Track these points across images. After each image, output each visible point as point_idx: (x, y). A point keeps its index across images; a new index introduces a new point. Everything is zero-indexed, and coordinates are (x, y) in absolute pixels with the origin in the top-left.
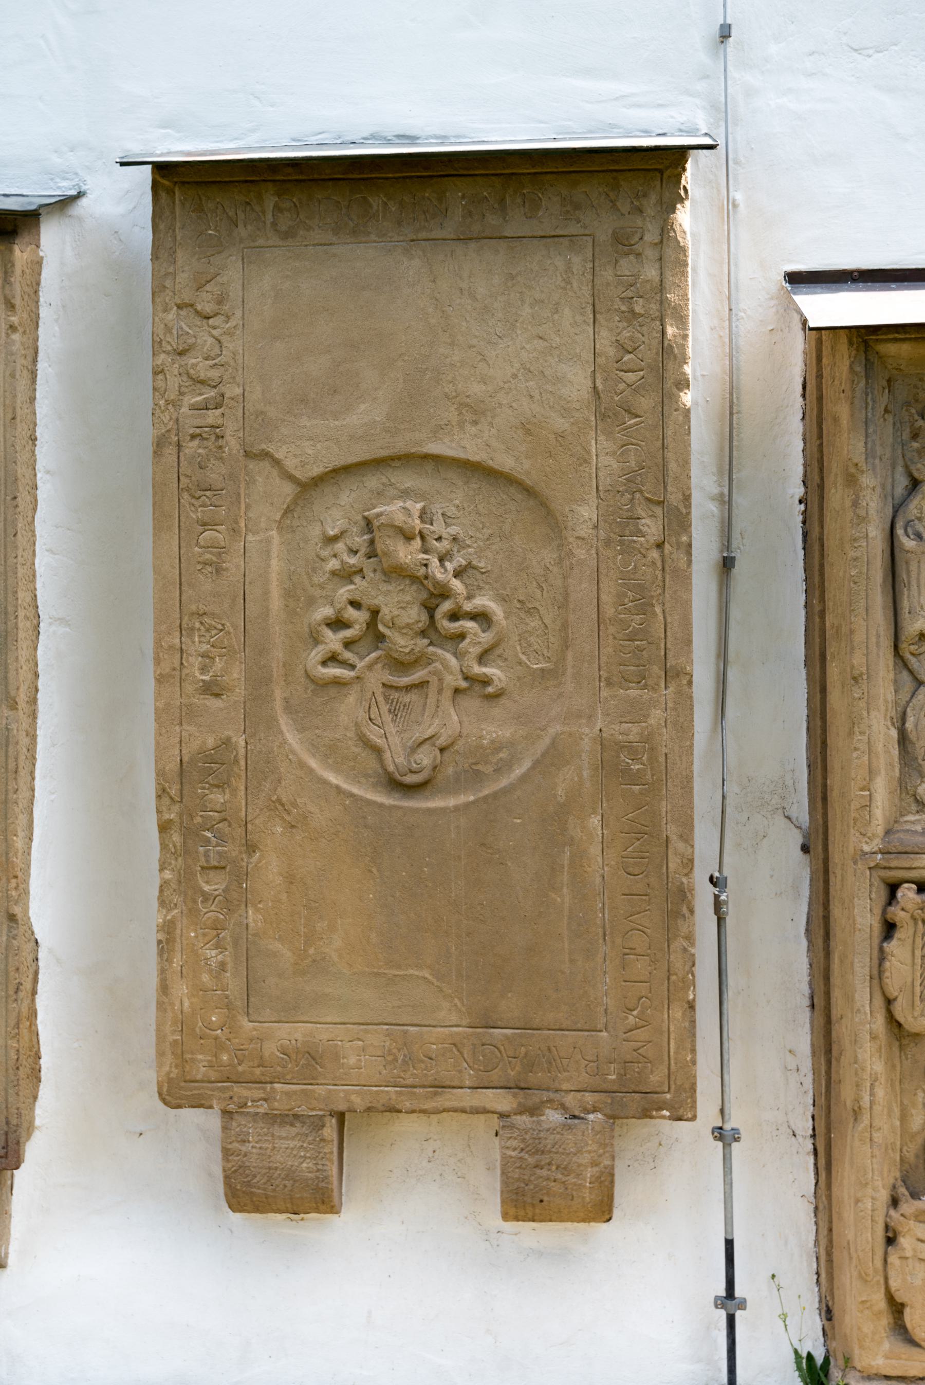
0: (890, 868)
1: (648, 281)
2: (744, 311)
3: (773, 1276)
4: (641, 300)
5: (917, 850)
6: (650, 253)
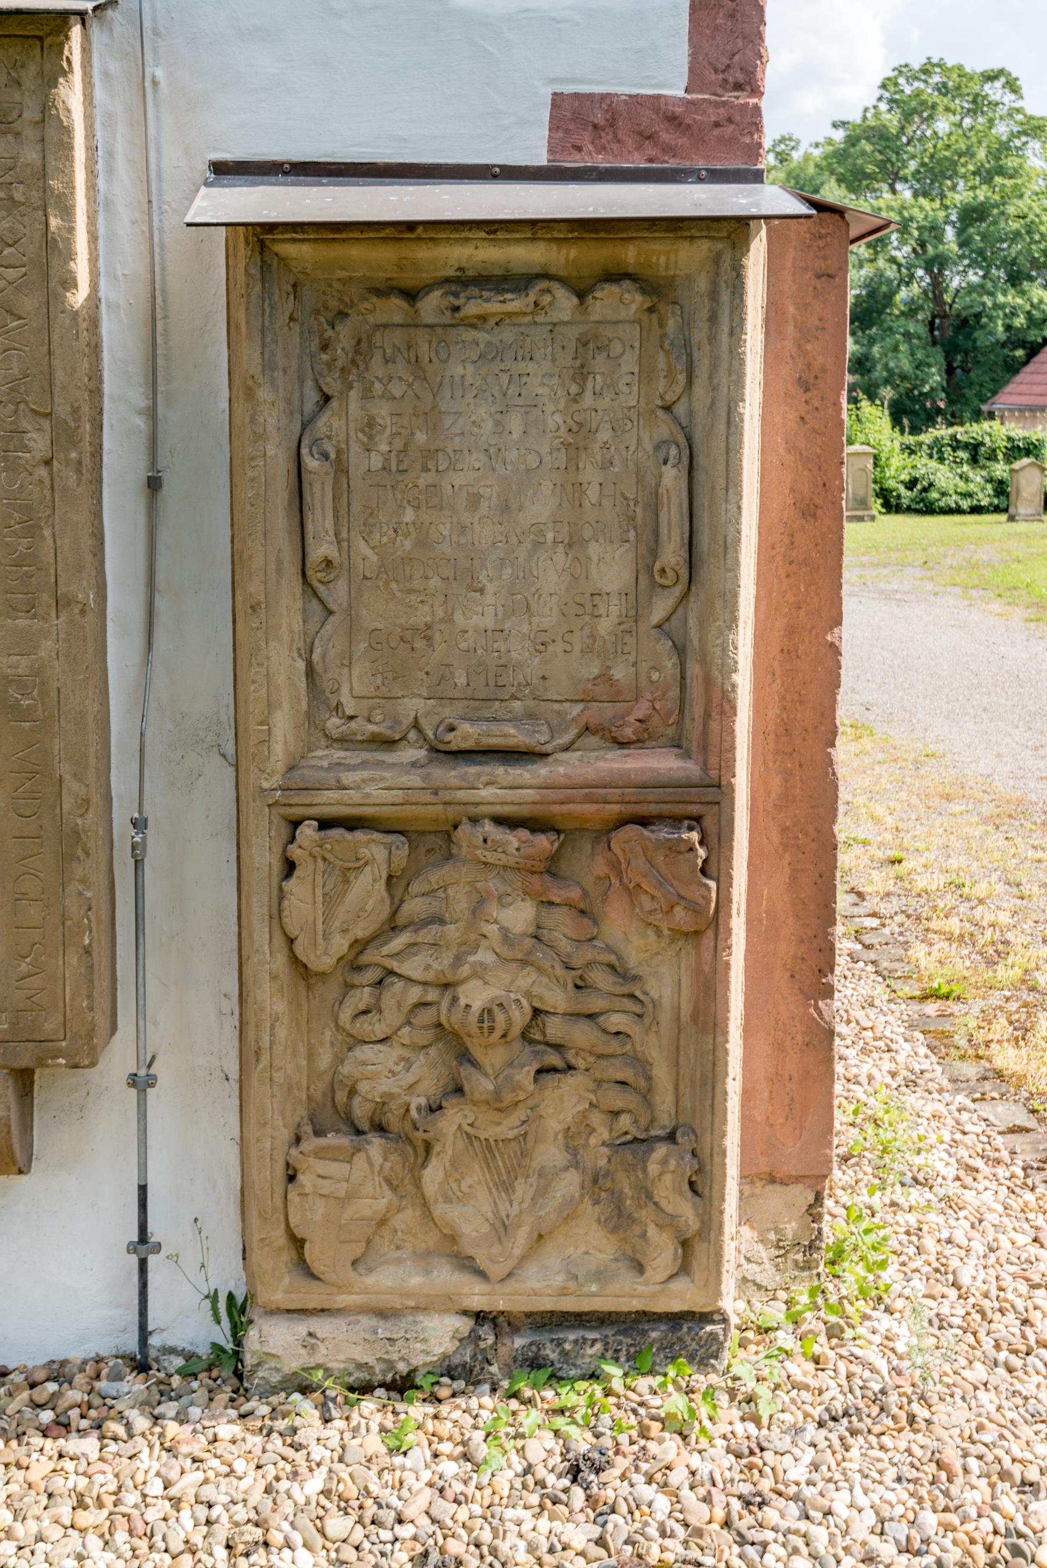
0: (290, 805)
1: (28, 165)
2: (168, 203)
3: (196, 1220)
4: (21, 186)
5: (318, 786)
6: (30, 133)
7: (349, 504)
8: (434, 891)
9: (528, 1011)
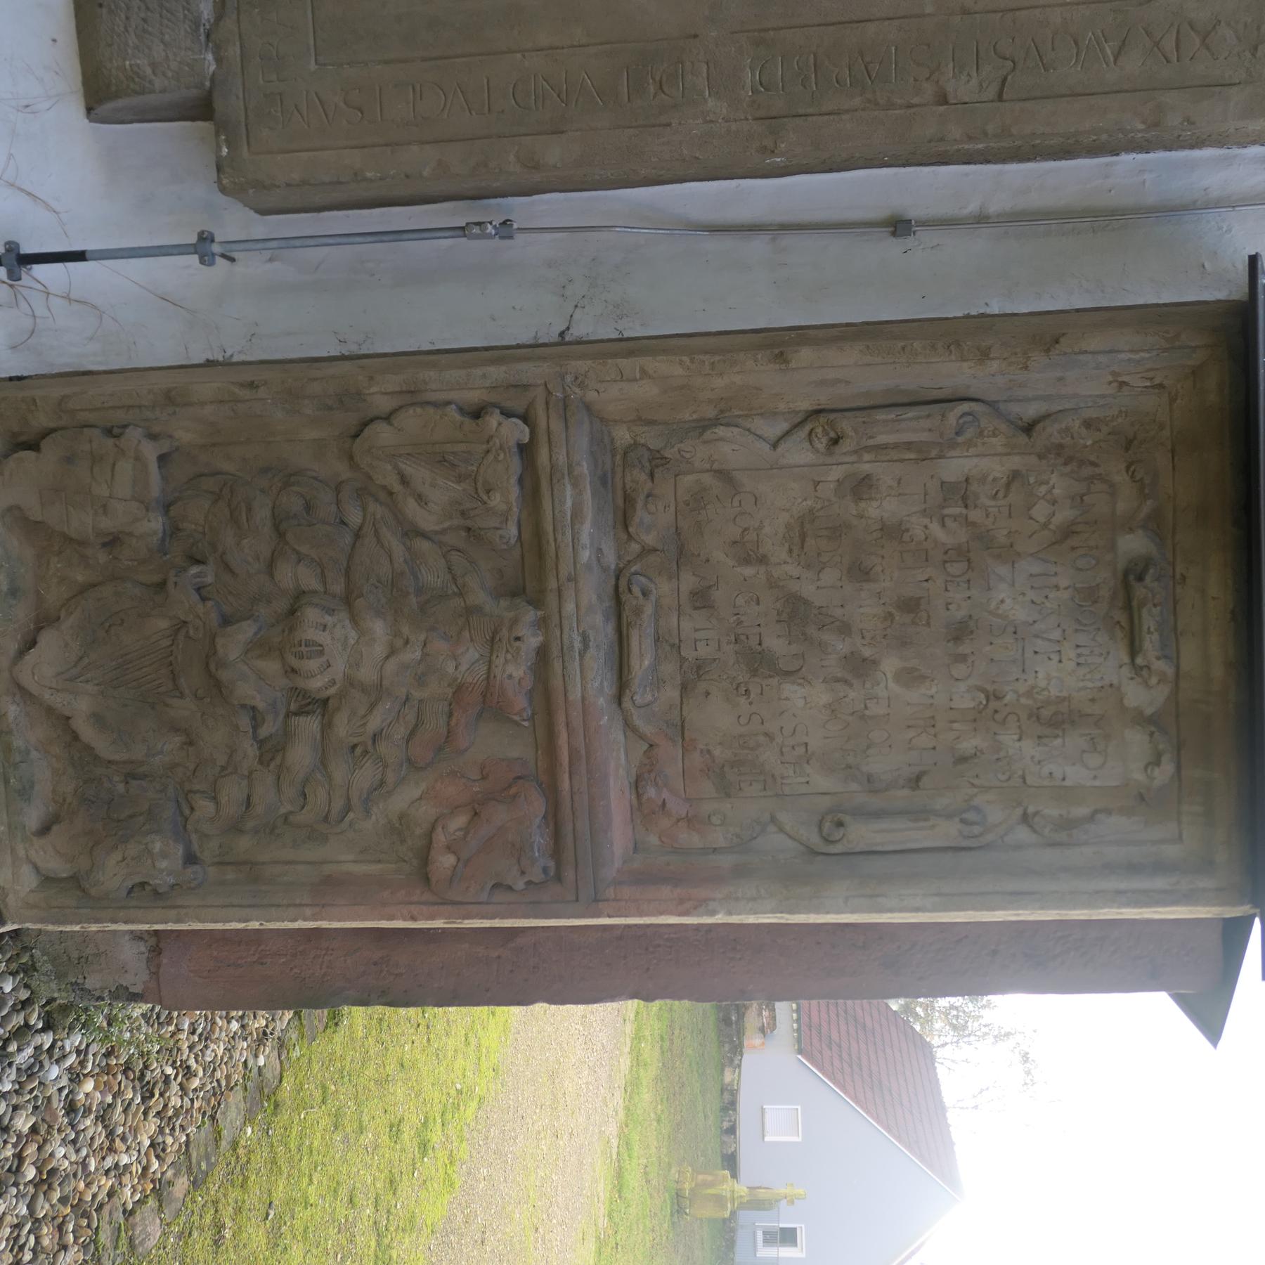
7: (902, 461)
8: (454, 579)
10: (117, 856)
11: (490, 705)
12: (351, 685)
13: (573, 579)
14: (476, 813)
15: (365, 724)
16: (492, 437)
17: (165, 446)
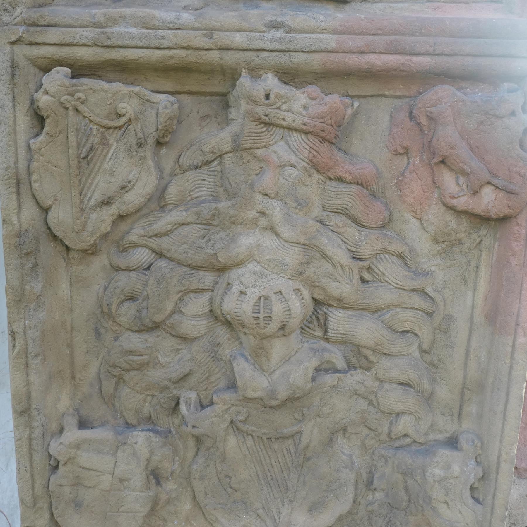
8: (207, 163)
9: (309, 302)
10: (443, 509)
11: (332, 134)
12: (301, 274)
13: (210, 31)
14: (443, 162)
15: (342, 266)
16: (61, 103)
17: (71, 422)
